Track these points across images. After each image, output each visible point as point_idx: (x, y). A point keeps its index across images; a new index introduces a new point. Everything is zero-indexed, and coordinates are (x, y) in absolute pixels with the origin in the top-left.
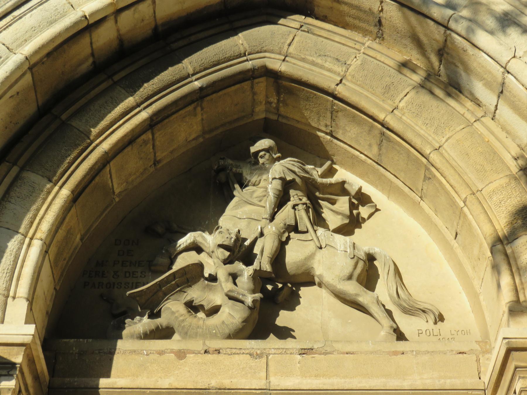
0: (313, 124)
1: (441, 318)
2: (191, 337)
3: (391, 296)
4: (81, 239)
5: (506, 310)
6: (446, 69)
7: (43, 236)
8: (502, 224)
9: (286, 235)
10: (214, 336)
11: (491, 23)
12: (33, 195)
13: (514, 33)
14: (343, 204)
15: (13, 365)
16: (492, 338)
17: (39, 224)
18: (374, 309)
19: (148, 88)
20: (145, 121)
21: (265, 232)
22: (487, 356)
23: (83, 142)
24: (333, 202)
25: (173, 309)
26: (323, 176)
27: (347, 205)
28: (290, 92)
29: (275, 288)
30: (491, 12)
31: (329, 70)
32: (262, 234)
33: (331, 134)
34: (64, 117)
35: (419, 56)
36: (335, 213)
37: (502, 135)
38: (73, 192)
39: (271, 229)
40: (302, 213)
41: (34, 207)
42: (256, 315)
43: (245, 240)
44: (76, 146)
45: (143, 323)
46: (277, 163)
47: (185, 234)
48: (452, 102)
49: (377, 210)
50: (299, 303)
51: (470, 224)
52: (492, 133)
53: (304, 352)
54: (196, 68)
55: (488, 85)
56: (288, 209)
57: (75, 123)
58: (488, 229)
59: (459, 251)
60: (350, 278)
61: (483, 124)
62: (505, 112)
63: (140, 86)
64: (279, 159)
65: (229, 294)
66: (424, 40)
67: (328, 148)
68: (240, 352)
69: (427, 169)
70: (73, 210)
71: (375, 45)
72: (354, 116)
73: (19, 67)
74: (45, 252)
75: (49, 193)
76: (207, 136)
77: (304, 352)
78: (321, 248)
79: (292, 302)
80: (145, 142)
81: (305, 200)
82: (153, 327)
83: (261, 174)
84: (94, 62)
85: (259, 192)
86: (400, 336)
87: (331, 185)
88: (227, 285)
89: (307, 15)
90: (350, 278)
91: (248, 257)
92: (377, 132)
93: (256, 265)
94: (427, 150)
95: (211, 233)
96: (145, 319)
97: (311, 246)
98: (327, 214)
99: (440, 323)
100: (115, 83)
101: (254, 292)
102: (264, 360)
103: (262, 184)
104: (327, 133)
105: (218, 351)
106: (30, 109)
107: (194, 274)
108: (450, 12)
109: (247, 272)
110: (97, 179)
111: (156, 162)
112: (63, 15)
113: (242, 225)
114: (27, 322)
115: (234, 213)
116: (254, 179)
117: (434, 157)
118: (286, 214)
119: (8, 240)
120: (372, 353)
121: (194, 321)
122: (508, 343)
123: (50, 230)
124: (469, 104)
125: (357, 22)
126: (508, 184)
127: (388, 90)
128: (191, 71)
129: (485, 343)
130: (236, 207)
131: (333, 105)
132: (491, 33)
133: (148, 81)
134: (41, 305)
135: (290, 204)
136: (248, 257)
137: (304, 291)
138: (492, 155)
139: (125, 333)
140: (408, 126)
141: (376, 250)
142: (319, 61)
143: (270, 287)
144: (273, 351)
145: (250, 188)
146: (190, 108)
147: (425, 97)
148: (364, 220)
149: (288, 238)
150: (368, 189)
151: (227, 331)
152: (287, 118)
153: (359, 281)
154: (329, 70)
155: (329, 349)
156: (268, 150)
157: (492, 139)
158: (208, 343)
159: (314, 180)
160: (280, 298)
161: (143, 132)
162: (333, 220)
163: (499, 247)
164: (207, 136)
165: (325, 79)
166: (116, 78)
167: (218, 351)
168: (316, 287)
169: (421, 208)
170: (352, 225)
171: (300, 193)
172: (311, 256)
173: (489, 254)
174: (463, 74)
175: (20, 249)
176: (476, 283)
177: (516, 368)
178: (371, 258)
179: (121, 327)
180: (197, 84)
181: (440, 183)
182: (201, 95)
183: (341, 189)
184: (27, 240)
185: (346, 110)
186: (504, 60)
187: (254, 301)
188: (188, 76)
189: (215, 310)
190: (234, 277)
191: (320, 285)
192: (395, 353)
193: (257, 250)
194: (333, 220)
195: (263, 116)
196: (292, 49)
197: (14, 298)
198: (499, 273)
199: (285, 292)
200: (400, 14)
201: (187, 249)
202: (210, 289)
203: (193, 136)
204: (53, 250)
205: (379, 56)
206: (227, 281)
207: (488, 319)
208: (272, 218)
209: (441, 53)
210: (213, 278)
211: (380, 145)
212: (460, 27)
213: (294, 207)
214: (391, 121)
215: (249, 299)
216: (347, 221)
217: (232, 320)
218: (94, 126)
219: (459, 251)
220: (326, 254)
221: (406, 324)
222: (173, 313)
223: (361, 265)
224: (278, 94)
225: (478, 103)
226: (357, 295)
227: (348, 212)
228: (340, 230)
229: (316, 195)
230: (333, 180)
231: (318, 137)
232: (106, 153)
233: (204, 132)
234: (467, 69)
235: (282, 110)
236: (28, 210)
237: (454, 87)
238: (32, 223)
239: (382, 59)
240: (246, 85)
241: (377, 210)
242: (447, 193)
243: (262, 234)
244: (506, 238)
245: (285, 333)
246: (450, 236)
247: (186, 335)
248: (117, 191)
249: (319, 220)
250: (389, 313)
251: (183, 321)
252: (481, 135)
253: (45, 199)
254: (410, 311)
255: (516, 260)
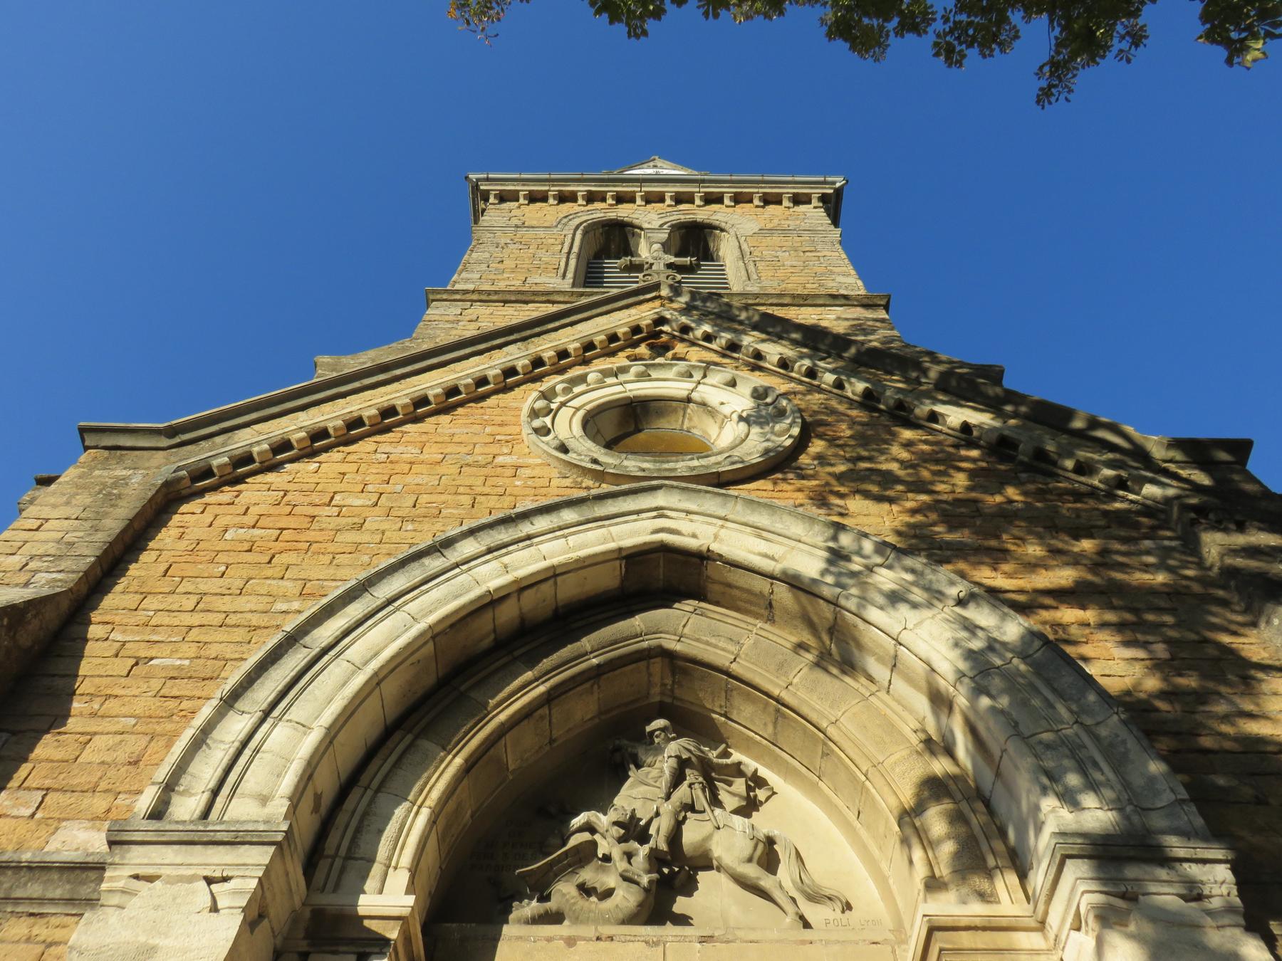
0: (709, 706)
1: (848, 907)
2: (582, 922)
3: (793, 882)
4: (472, 817)
5: (921, 886)
6: (836, 646)
7: (432, 804)
8: (907, 795)
9: (683, 814)
10: (607, 922)
11: (880, 600)
12: (427, 763)
13: (904, 609)
14: (739, 785)
15: (385, 942)
16: (907, 926)
17: (429, 792)
18: (777, 895)
19: (547, 663)
20: (542, 694)
21: (661, 811)
22: (903, 947)
23: (480, 712)
24: (730, 784)
25: (564, 890)
26: (719, 757)
27: (744, 787)
28: (685, 672)
29: (672, 871)
30: (880, 591)
31: (723, 649)
32: (657, 814)
33: (725, 715)
34: (463, 688)
35: (810, 637)
36: (732, 794)
37: (899, 709)
38: (466, 761)
39: (667, 808)
40: (698, 792)
41: (426, 775)
42: (651, 899)
43: (641, 819)
44: (474, 716)
45: (531, 907)
46: (673, 743)
47: (578, 815)
48: (847, 679)
49: (774, 793)
50: (697, 889)
51: (873, 799)
52: (888, 706)
53: (704, 940)
54: (593, 647)
55: (880, 660)
56: (684, 787)
57: (473, 694)
58: (893, 802)
59: (863, 833)
60: (750, 860)
61: (879, 698)
62: (899, 685)
63: (539, 661)
64: (674, 739)
65: (621, 876)
66: (815, 619)
67: (722, 731)
68: (633, 939)
69: (825, 744)
70: (465, 781)
71: (767, 626)
72: (749, 694)
73: (422, 635)
74: (432, 822)
75: (442, 761)
76: (603, 717)
77: (704, 940)
78: (718, 828)
79: (689, 887)
80: (542, 718)
81: (701, 779)
82: (542, 911)
83: (656, 755)
84: (495, 639)
85: (654, 772)
86: (807, 925)
87: (727, 765)
88: (620, 864)
89: (700, 600)
90: (750, 860)
91: (643, 837)
92: (771, 710)
93: (652, 843)
94: (824, 724)
95: (605, 814)
96: (534, 903)
97: (708, 827)
98: (723, 796)
99: (847, 912)
100: (516, 659)
101: (649, 872)
102: (661, 948)
103: (658, 764)
104: (721, 715)
105: (611, 938)
106: (430, 680)
107: (586, 854)
108: (839, 590)
109: (643, 851)
110: (492, 751)
111: (552, 741)
112: (468, 591)
113: (637, 805)
114: (407, 893)
115: (629, 793)
116: (649, 760)
117: (831, 731)
118: (682, 792)
119: (396, 807)
120: (777, 941)
121: (587, 904)
122: (929, 921)
123: (440, 799)
124: (863, 680)
125: (748, 606)
126: (909, 756)
127: (781, 667)
128: (589, 648)
129: (899, 929)
130: (632, 787)
131: (727, 683)
132: (881, 608)
133: (547, 657)
134: (422, 879)
135: (686, 783)
136: (643, 837)
137: (702, 876)
138: (891, 728)
139: (511, 917)
140: (804, 701)
141: (775, 833)
142: (713, 641)
143: (666, 871)
144: (670, 938)
145: (645, 769)
146: (587, 685)
147: (820, 675)
148: (761, 803)
149: (685, 818)
150: (764, 772)
151: (621, 916)
152: (681, 700)
153: (759, 863)
154: (723, 649)
155: (731, 938)
156: (663, 729)
157: (889, 712)
158: (600, 928)
159: (710, 760)
160: (677, 882)
161: (540, 706)
162: (730, 802)
163: (907, 819)
164: (603, 717)
165: (720, 657)
166: (516, 653)
167: (611, 938)
168: (714, 872)
169: (820, 789)
170: (749, 807)
171: (696, 773)
172: (708, 838)
173: (897, 828)
174: (855, 651)
175: (406, 817)
176: (884, 866)
177: (941, 950)
178: (770, 841)
179: (508, 910)
180: (595, 661)
181: (839, 758)
182: (599, 671)
183: (737, 770)
184: (415, 808)
185: (740, 688)
186: (895, 632)
187: (650, 882)
188: (586, 654)
189: (608, 893)
190: (629, 856)
191: (718, 870)
192: (803, 942)
193: (652, 831)
194: (730, 802)
195: (657, 699)
196: (686, 631)
197: (396, 868)
198: (910, 847)
199: (682, 876)
200: (790, 595)
201: (581, 830)
202: (603, 869)
203: (589, 717)
204: (441, 821)
205: (771, 636)
206: (621, 860)
207: (900, 905)
208: (668, 797)
209: (831, 631)
210: (607, 858)
211: (775, 724)
212: (851, 604)
213: (690, 786)
214: (785, 696)
215: (645, 880)
216: (744, 803)
217: (626, 904)
218: (492, 698)
219: (863, 833)
220: (724, 836)
221: (813, 912)
222: (564, 895)
223: (761, 846)
224: (673, 674)
225: (871, 679)
226: (758, 878)
227: (745, 794)
228: (737, 812)
229: (712, 776)
230: (729, 761)
231: (713, 719)
232: (502, 724)
233: (600, 713)
234: (860, 646)
235: (678, 692)
236: (419, 777)
237: (849, 666)
238: (422, 791)
239: (775, 638)
240: (643, 664)
241: (774, 793)
242: (847, 767)
243: (657, 814)
244: (912, 809)
245: (683, 920)
246: (852, 816)
247: (576, 920)
248: (511, 768)
249: (715, 802)
250: (794, 900)
251: (574, 904)
252: (877, 709)
253: (437, 768)
254: (815, 897)
255: (926, 832)
